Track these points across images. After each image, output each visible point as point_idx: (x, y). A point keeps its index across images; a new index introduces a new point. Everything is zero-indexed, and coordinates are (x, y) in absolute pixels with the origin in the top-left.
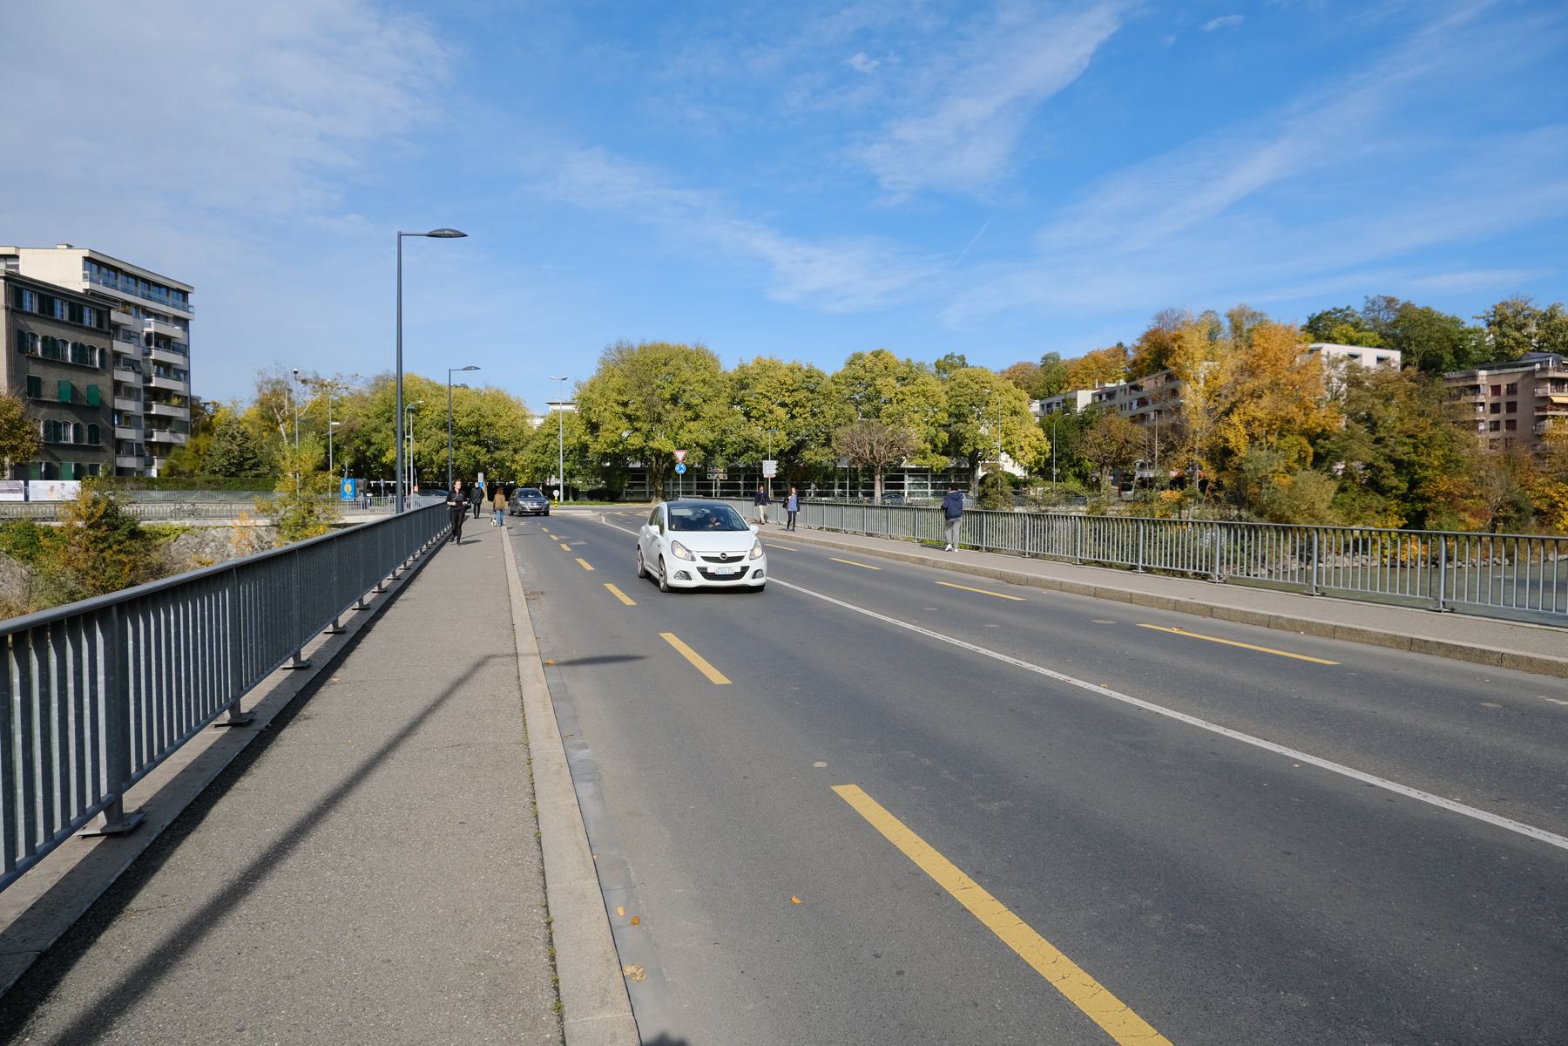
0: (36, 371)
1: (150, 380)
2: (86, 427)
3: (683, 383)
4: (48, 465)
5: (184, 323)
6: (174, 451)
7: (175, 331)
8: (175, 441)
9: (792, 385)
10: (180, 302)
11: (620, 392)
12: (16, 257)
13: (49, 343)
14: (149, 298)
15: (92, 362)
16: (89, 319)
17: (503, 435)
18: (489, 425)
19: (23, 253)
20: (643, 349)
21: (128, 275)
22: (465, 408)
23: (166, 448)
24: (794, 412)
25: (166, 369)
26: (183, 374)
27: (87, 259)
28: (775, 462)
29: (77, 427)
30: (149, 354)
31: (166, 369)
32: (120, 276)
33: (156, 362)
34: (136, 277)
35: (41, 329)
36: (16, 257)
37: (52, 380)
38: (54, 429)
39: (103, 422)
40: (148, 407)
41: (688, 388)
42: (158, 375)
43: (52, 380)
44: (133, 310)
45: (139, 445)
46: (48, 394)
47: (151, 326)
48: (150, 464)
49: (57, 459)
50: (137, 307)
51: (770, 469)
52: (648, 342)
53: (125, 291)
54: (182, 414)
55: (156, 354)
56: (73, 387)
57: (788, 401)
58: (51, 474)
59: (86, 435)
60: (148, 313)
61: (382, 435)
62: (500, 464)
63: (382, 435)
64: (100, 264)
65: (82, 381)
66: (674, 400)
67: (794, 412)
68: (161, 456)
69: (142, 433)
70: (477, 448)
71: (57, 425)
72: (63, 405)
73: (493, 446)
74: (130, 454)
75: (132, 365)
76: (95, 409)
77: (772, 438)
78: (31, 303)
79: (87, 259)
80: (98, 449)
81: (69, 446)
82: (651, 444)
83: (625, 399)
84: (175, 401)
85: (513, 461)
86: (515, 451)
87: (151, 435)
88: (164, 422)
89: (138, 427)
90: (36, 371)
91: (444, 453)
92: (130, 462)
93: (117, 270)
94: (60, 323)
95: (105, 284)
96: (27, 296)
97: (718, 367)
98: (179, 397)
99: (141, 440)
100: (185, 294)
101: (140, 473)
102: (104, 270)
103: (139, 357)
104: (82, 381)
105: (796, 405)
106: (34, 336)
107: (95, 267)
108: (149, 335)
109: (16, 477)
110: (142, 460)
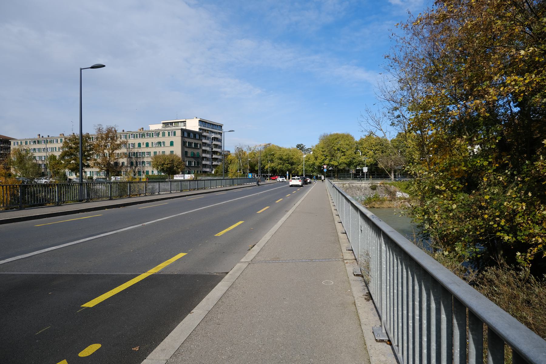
0: (186, 149)
1: (212, 149)
2: (196, 162)
3: (340, 145)
4: (189, 171)
5: (221, 134)
6: (218, 167)
7: (218, 136)
8: (218, 164)
9: (375, 144)
10: (220, 129)
11: (323, 148)
12: (185, 121)
13: (190, 144)
14: (213, 128)
15: (198, 147)
16: (197, 137)
17: (295, 161)
18: (291, 158)
19: (187, 121)
20: (331, 135)
21: (208, 123)
22: (285, 154)
23: (216, 166)
24: (376, 152)
25: (216, 146)
26: (220, 147)
27: (199, 121)
28: (367, 168)
29: (194, 162)
30: (212, 143)
31: (216, 146)
32: (207, 124)
33: (214, 144)
34: (210, 124)
35: (188, 140)
36: (185, 121)
37: (190, 151)
38: (190, 163)
39: (200, 160)
40: (212, 156)
41: (342, 146)
42: (215, 148)
43: (190, 151)
44: (209, 132)
45: (210, 165)
46: (189, 155)
47: (213, 136)
48: (212, 170)
49: (190, 170)
50: (210, 131)
51: (365, 170)
52: (332, 133)
53: (208, 127)
54: (220, 157)
55: (214, 143)
56: (194, 153)
57: (374, 149)
58: (189, 173)
59: (196, 164)
60: (213, 132)
61: (264, 162)
62: (294, 169)
63: (264, 162)
64: (202, 121)
65: (196, 151)
66: (338, 149)
67: (376, 152)
68: (215, 168)
69: (211, 162)
70: (288, 165)
71: (191, 162)
72: (192, 157)
73: (292, 164)
74: (208, 168)
75: (209, 145)
76: (198, 158)
77: (367, 160)
78: (186, 135)
79: (199, 121)
80: (199, 167)
81: (193, 166)
82: (331, 163)
83: (324, 150)
84: (218, 154)
85: (297, 168)
86: (298, 165)
87: (213, 163)
88: (216, 159)
89: (210, 161)
90: (186, 149)
91: (280, 166)
92: (208, 170)
93: (206, 122)
94: (192, 138)
95: (203, 126)
96: (185, 133)
97: (354, 140)
98: (219, 153)
99: (211, 164)
100: (221, 126)
101: (210, 172)
102: (203, 123)
103: (210, 144)
104: (196, 151)
105: (376, 150)
106: (186, 142)
107: (201, 122)
108: (213, 138)
109: (182, 174)
110: (211, 169)
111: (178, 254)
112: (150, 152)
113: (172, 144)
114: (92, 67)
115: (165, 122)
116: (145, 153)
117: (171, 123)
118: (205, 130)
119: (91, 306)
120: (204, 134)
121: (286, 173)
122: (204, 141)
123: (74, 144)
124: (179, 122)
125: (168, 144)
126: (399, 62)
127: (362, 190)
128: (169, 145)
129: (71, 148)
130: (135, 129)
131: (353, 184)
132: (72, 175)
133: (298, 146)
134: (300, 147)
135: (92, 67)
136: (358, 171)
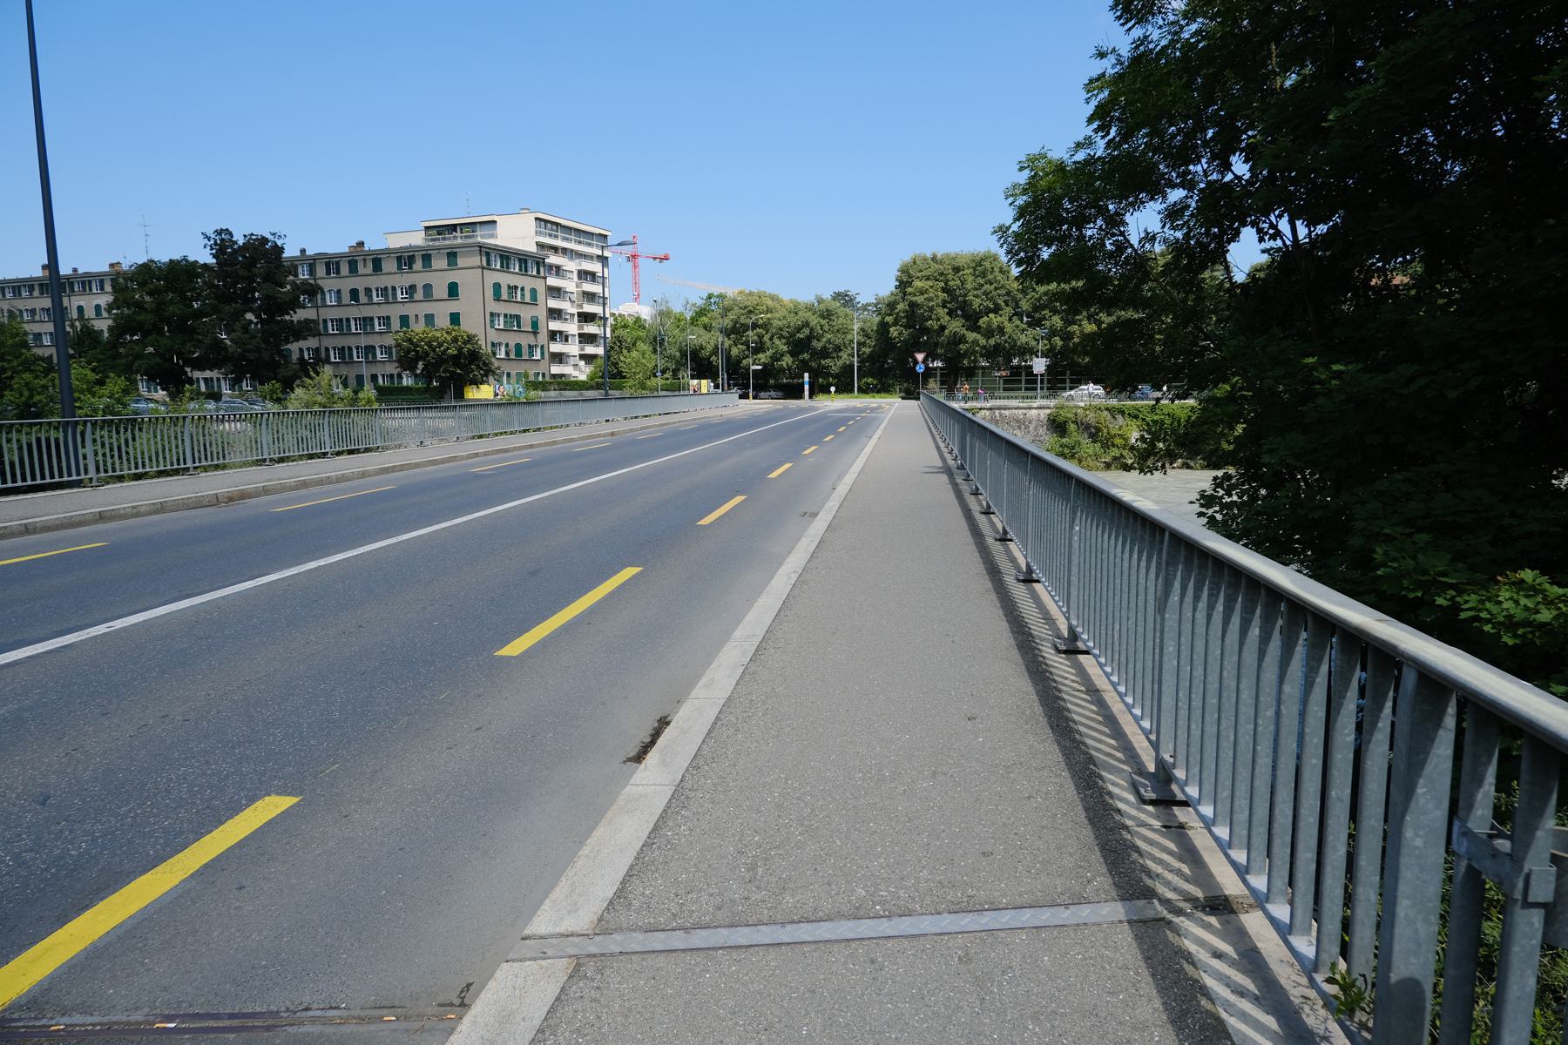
25: (590, 297)
31: (590, 297)
51: (1039, 365)
102: (549, 225)
111: (252, 800)
112: (388, 318)
113: (453, 290)
114: (619, 245)
115: (432, 224)
116: (372, 319)
117: (453, 228)
118: (555, 249)
119: (515, 653)
120: (553, 259)
121: (803, 377)
122: (553, 281)
123: (150, 294)
124: (475, 223)
125: (441, 291)
126: (977, 289)
127: (1031, 428)
128: (348, 274)
129: (140, 305)
130: (338, 245)
131: (1003, 411)
132: (157, 391)
133: (838, 296)
134: (845, 299)
135: (619, 245)
136: (1016, 371)
